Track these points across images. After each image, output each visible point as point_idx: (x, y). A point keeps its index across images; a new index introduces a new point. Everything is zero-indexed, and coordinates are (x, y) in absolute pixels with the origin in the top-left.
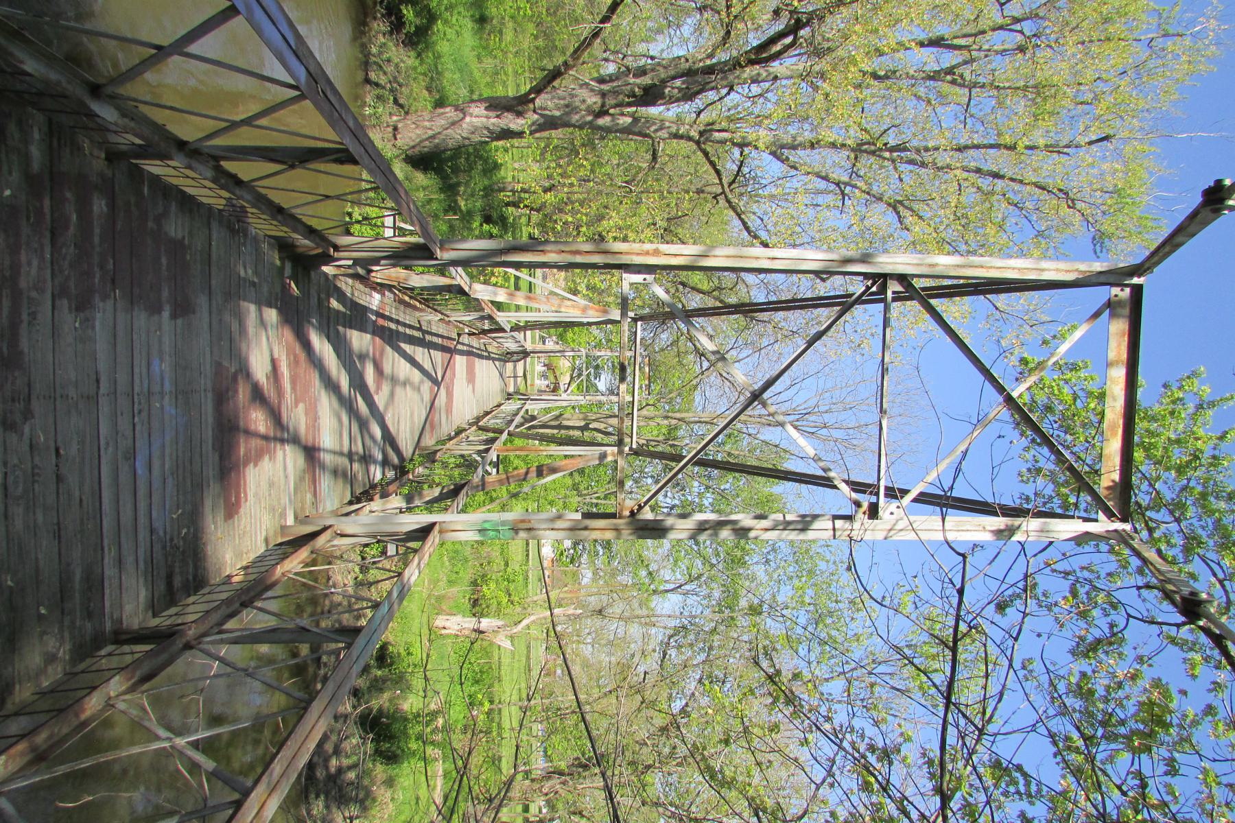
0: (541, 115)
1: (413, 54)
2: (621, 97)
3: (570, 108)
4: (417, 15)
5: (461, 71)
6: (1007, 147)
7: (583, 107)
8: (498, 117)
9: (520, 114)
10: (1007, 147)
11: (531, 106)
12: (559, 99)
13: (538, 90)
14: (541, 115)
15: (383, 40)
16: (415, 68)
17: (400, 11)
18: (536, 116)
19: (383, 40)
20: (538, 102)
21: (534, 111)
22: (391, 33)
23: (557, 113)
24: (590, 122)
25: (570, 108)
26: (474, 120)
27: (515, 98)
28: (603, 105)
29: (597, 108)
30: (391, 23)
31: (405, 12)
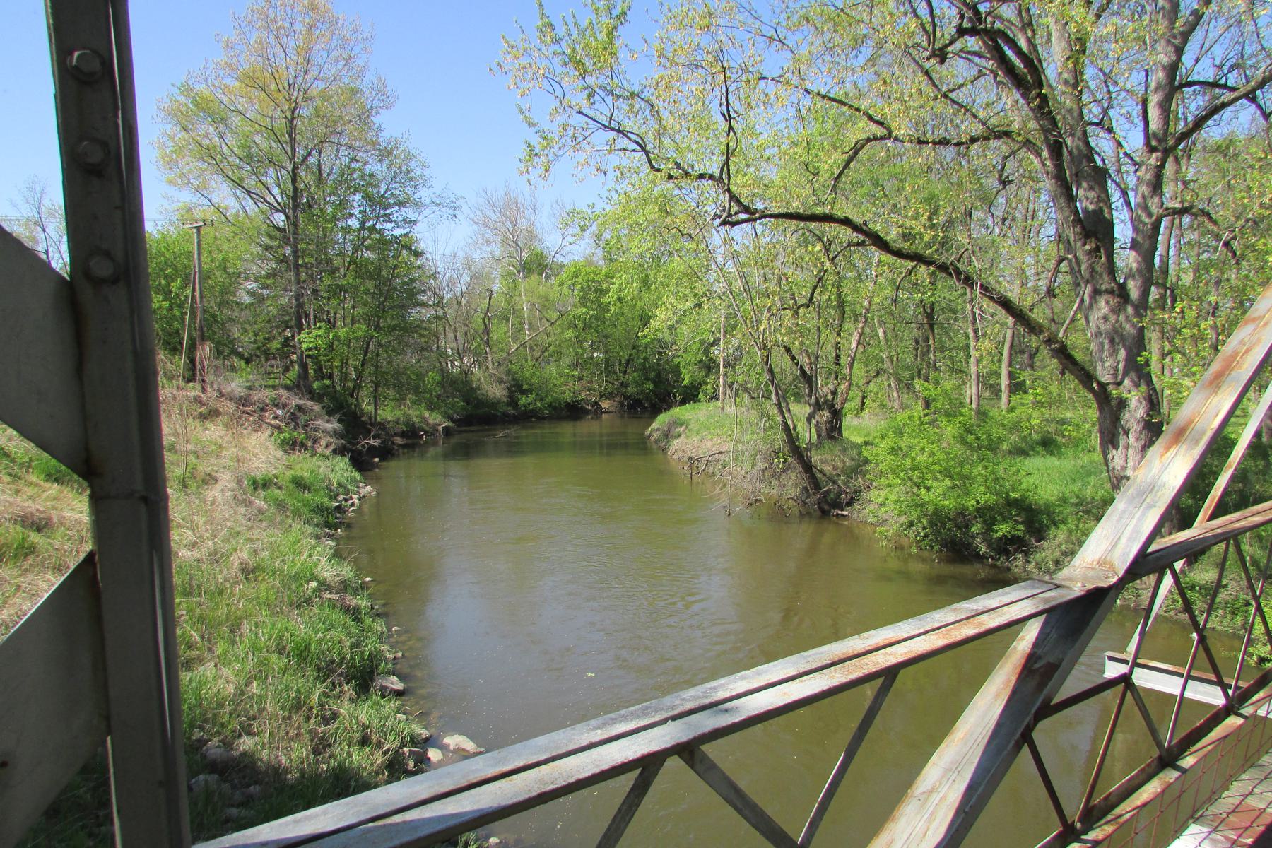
0: (1125, 374)
1: (1053, 531)
2: (1098, 268)
3: (1115, 337)
4: (1005, 519)
5: (1089, 474)
6: (1147, 76)
7: (1112, 318)
8: (1126, 433)
9: (1123, 403)
10: (1147, 76)
11: (1110, 388)
12: (1102, 350)
13: (1086, 377)
14: (1125, 374)
15: (1033, 565)
16: (1070, 531)
17: (1001, 539)
18: (1126, 382)
19: (1033, 565)
20: (1106, 379)
21: (1119, 384)
22: (1026, 553)
23: (1122, 353)
24: (1136, 308)
25: (1115, 337)
26: (1130, 465)
27: (1100, 409)
28: (1111, 292)
29: (1113, 301)
30: (1016, 551)
31: (1000, 534)
